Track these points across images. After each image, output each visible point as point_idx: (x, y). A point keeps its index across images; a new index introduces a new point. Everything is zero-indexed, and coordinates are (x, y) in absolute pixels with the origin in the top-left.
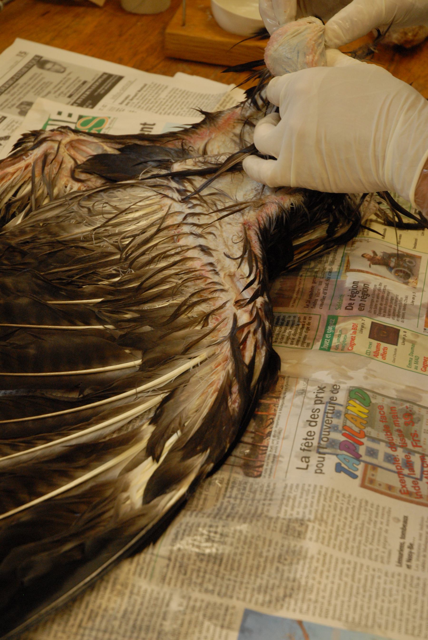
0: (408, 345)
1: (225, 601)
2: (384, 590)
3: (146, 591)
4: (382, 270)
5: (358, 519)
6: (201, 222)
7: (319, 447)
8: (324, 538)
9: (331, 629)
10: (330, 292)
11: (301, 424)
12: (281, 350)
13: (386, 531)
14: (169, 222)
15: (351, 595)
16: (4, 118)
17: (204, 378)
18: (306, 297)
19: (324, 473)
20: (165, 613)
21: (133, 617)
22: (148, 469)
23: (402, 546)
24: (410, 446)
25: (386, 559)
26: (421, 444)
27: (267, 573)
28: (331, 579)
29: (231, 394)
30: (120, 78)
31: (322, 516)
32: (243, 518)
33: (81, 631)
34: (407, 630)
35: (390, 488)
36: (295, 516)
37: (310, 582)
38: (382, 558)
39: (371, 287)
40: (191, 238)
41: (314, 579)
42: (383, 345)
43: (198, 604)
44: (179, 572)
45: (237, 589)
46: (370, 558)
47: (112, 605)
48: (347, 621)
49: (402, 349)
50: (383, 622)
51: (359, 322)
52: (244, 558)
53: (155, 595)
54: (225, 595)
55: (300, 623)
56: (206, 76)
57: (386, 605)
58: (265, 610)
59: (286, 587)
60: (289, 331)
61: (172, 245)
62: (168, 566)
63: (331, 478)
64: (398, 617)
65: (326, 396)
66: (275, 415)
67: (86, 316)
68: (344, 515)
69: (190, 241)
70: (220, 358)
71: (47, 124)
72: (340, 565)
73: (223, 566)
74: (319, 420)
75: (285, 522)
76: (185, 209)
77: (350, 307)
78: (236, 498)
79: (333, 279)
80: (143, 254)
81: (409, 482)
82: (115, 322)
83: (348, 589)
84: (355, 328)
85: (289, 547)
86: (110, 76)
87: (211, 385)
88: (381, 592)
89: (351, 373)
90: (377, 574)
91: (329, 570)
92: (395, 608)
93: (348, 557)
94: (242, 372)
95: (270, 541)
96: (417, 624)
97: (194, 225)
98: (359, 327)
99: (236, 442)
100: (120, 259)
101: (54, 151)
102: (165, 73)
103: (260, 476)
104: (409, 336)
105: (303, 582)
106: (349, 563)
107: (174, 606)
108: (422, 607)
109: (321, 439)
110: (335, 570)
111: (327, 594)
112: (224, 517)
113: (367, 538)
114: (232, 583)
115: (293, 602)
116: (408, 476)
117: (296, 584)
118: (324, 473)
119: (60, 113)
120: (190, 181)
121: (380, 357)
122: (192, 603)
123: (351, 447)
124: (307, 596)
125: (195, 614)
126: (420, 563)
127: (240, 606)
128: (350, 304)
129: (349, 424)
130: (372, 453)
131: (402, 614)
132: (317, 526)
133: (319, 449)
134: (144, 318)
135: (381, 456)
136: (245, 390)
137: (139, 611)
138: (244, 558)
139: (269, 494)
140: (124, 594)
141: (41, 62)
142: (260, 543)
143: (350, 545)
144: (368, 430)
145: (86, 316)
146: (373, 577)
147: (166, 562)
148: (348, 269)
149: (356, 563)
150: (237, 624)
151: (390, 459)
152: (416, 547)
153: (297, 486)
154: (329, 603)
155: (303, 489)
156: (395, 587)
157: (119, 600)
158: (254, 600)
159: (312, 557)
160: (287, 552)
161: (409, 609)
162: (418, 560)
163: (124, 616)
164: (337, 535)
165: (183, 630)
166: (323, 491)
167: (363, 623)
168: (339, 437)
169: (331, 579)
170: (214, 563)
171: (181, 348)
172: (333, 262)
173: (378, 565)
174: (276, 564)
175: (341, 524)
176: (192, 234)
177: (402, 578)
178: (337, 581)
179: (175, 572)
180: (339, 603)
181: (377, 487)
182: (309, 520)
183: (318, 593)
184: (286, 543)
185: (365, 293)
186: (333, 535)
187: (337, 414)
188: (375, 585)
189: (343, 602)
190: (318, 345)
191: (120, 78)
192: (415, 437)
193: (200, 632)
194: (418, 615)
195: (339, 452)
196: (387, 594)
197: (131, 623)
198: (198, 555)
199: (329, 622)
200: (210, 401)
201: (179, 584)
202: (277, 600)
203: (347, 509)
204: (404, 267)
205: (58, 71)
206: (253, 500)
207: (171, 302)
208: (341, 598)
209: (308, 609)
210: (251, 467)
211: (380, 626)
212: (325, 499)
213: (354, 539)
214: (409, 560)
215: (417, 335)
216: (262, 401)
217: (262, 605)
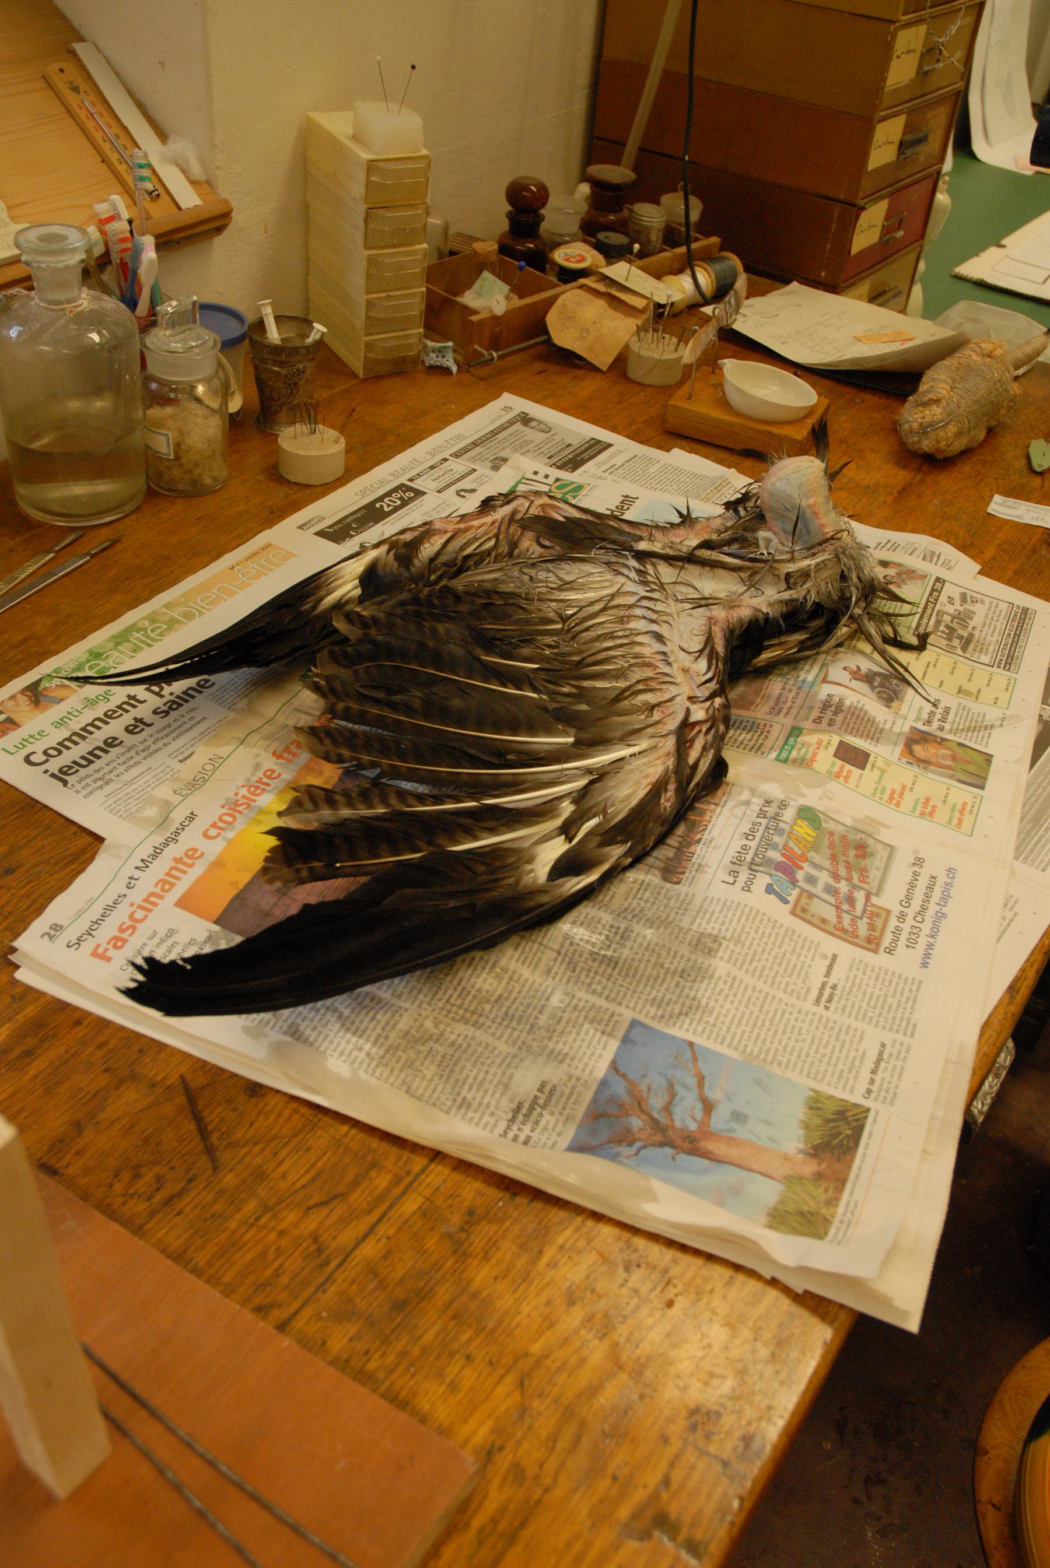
0: (877, 773)
1: (613, 1007)
2: (794, 1027)
3: (527, 980)
4: (863, 687)
5: (780, 947)
6: (657, 608)
7: (752, 863)
8: (737, 960)
9: (725, 1057)
10: (799, 701)
11: (737, 836)
12: (727, 755)
13: (810, 966)
14: (619, 601)
15: (755, 1025)
17: (638, 766)
18: (771, 703)
20: (543, 1007)
21: (508, 1004)
22: (556, 849)
23: (824, 984)
24: (856, 881)
25: (802, 995)
26: (870, 880)
27: (665, 985)
28: (736, 1004)
29: (666, 790)
30: (610, 445)
31: (740, 936)
32: (651, 923)
33: (448, 1006)
34: (809, 1073)
35: (824, 921)
36: (709, 931)
37: (712, 1003)
38: (799, 993)
39: (848, 703)
40: (643, 622)
41: (716, 1001)
42: (848, 767)
43: (581, 1004)
44: (568, 967)
45: (628, 996)
46: (785, 991)
47: (487, 987)
48: (744, 1052)
49: (869, 775)
50: (785, 1060)
51: (825, 737)
52: (643, 965)
53: (536, 986)
54: (614, 1000)
55: (691, 1044)
56: (707, 457)
57: (792, 1043)
58: (654, 1024)
59: (683, 1005)
60: (744, 736)
61: (621, 627)
62: (556, 960)
63: (759, 899)
64: (803, 1057)
65: (771, 810)
67: (518, 679)
68: (765, 940)
69: (641, 625)
70: (662, 752)
71: (519, 482)
72: (749, 992)
73: (617, 970)
74: (758, 835)
75: (697, 935)
76: (642, 591)
77: (818, 720)
78: (647, 901)
79: (805, 688)
80: (587, 629)
81: (847, 919)
82: (550, 693)
83: (753, 1019)
84: (819, 743)
85: (695, 962)
86: (599, 442)
87: (646, 777)
88: (789, 1029)
89: (804, 790)
90: (789, 1009)
91: (735, 996)
92: (802, 1048)
93: (760, 985)
94: (682, 772)
95: (676, 953)
96: (822, 1069)
97: (649, 609)
98: (825, 743)
99: (660, 841)
100: (562, 629)
101: (523, 510)
102: (660, 448)
103: (679, 883)
104: (880, 763)
105: (703, 1004)
106: (760, 992)
107: (555, 1001)
108: (832, 1052)
109: (756, 855)
110: (743, 996)
111: (728, 1021)
112: (629, 917)
113: (786, 969)
114: (624, 990)
115: (688, 1021)
116: (847, 912)
117: (696, 1003)
119: (536, 473)
120: (654, 565)
121: (841, 780)
122: (575, 1002)
123: (788, 869)
124: (705, 1018)
125: (576, 1014)
126: (840, 1006)
127: (628, 1015)
128: (820, 718)
129: (791, 844)
130: (811, 880)
131: (807, 1055)
132: (731, 946)
133: (752, 866)
134: (581, 695)
135: (821, 885)
136: (681, 789)
137: (515, 999)
138: (643, 965)
139: (685, 905)
140: (502, 978)
141: (525, 419)
142: (664, 953)
143: (766, 972)
144: (811, 855)
145: (518, 679)
146: (784, 1011)
147: (555, 955)
148: (825, 680)
149: (767, 994)
150: (621, 1033)
152: (839, 988)
153: (719, 900)
154: (728, 1030)
155: (724, 905)
156: (806, 1026)
157: (495, 984)
158: (644, 1012)
159: (720, 978)
160: (692, 968)
161: (816, 1052)
162: (838, 1002)
163: (496, 1001)
164: (752, 960)
165: (559, 1028)
166: (747, 910)
167: (762, 1057)
168: (776, 856)
169: (736, 1004)
171: (618, 734)
172: (809, 671)
173: (793, 1000)
174: (677, 978)
175: (760, 949)
176: (644, 617)
177: (816, 1019)
178: (742, 1008)
179: (563, 968)
180: (739, 1032)
181: (809, 917)
182: (724, 938)
183: (718, 1017)
184: (693, 958)
185: (839, 708)
186: (748, 960)
187: (779, 832)
188: (784, 1021)
189: (744, 1031)
190: (773, 755)
191: (610, 445)
192: (864, 872)
193: (578, 1034)
194: (826, 1059)
195: (774, 872)
196: (796, 1032)
197: (504, 1010)
198: (591, 953)
199: (724, 1050)
200: (642, 793)
201: (565, 980)
202: (671, 1017)
203: (770, 934)
206: (666, 906)
207: (614, 684)
208: (742, 1027)
209: (703, 1032)
210: (671, 872)
211: (779, 1064)
212: (747, 919)
213: (771, 968)
214: (829, 1001)
215: (889, 763)
216: (698, 805)
217: (653, 1018)
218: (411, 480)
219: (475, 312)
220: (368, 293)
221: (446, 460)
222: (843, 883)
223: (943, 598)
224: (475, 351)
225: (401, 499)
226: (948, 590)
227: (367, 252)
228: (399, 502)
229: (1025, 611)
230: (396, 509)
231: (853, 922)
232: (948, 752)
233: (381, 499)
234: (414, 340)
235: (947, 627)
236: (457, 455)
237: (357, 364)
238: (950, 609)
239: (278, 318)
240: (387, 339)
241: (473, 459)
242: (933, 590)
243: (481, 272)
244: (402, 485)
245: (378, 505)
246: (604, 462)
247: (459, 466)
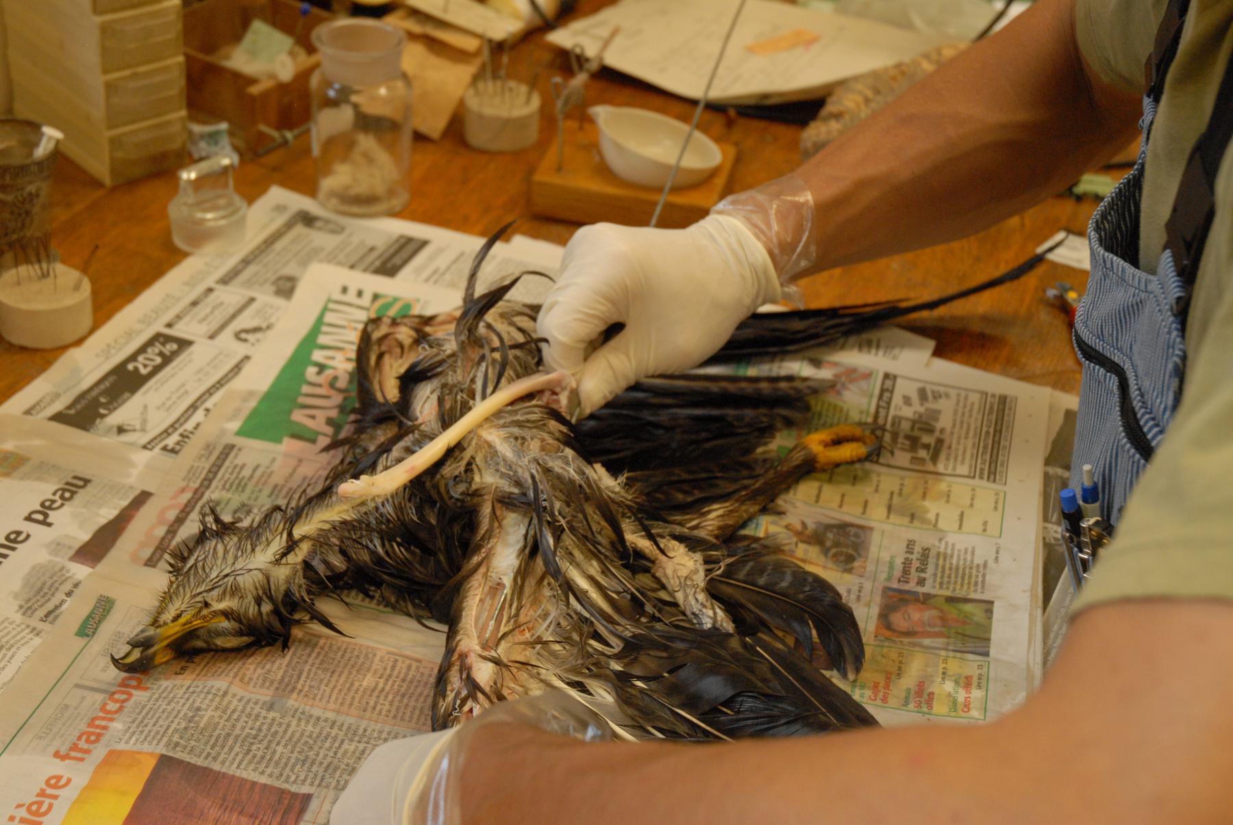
16: (252, 300)
19: (50, 525)
30: (424, 243)
71: (325, 309)
86: (410, 240)
118: (50, 525)
191: (424, 243)
204: (847, 546)
205: (333, 232)
218: (169, 325)
219: (252, 81)
220: (106, 71)
221: (210, 290)
223: (897, 399)
224: (261, 135)
225: (161, 354)
226: (903, 388)
227: (99, 19)
228: (159, 360)
229: (1003, 399)
230: (157, 369)
232: (934, 613)
233: (133, 357)
234: (176, 128)
235: (907, 437)
236: (225, 281)
237: (100, 168)
238: (908, 412)
240: (138, 131)
241: (249, 284)
242: (883, 391)
243: (245, 25)
247: (231, 296)
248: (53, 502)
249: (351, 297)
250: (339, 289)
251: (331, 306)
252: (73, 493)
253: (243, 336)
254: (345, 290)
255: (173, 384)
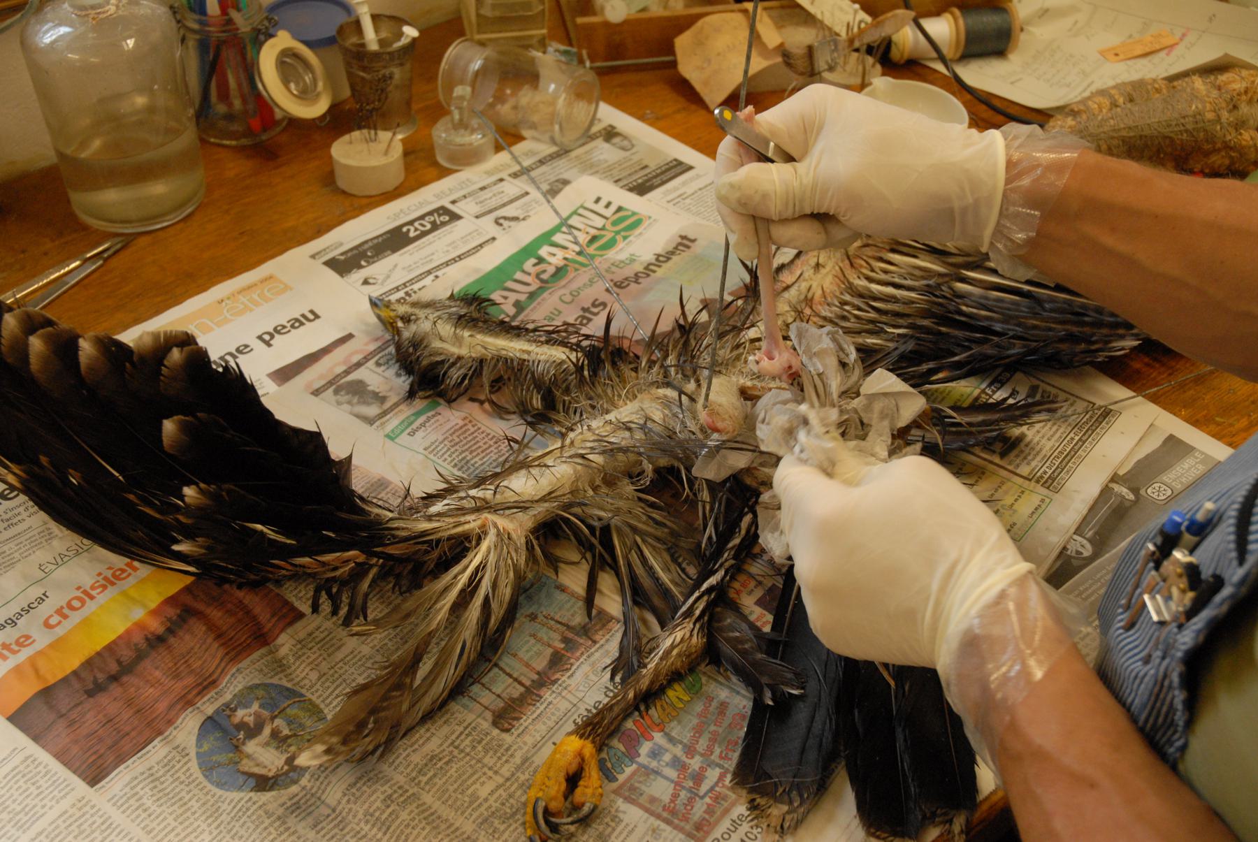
16: (527, 193)
30: (691, 168)
62: (328, 816)
66: (578, 659)
86: (680, 163)
103: (507, 730)
147: (329, 811)
151: (676, 763)
170: (379, 829)
191: (691, 168)
218: (453, 202)
221: (501, 180)
222: (698, 759)
230: (424, 234)
231: (691, 801)
233: (411, 223)
239: (375, 18)
244: (443, 208)
245: (405, 229)
246: (676, 189)
248: (284, 327)
249: (599, 208)
250: (594, 198)
251: (581, 211)
252: (302, 324)
253: (501, 221)
254: (598, 200)
255: (424, 252)
